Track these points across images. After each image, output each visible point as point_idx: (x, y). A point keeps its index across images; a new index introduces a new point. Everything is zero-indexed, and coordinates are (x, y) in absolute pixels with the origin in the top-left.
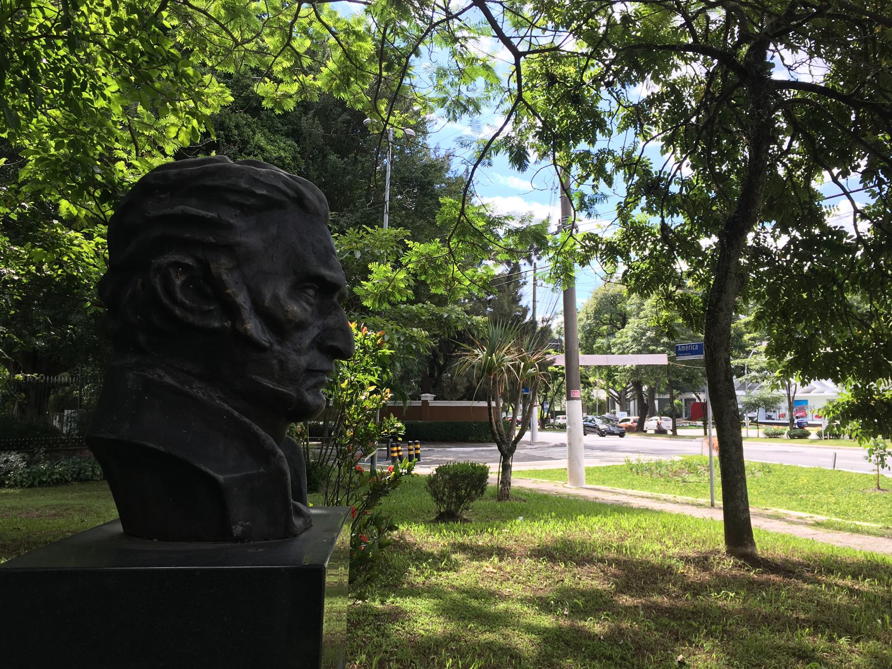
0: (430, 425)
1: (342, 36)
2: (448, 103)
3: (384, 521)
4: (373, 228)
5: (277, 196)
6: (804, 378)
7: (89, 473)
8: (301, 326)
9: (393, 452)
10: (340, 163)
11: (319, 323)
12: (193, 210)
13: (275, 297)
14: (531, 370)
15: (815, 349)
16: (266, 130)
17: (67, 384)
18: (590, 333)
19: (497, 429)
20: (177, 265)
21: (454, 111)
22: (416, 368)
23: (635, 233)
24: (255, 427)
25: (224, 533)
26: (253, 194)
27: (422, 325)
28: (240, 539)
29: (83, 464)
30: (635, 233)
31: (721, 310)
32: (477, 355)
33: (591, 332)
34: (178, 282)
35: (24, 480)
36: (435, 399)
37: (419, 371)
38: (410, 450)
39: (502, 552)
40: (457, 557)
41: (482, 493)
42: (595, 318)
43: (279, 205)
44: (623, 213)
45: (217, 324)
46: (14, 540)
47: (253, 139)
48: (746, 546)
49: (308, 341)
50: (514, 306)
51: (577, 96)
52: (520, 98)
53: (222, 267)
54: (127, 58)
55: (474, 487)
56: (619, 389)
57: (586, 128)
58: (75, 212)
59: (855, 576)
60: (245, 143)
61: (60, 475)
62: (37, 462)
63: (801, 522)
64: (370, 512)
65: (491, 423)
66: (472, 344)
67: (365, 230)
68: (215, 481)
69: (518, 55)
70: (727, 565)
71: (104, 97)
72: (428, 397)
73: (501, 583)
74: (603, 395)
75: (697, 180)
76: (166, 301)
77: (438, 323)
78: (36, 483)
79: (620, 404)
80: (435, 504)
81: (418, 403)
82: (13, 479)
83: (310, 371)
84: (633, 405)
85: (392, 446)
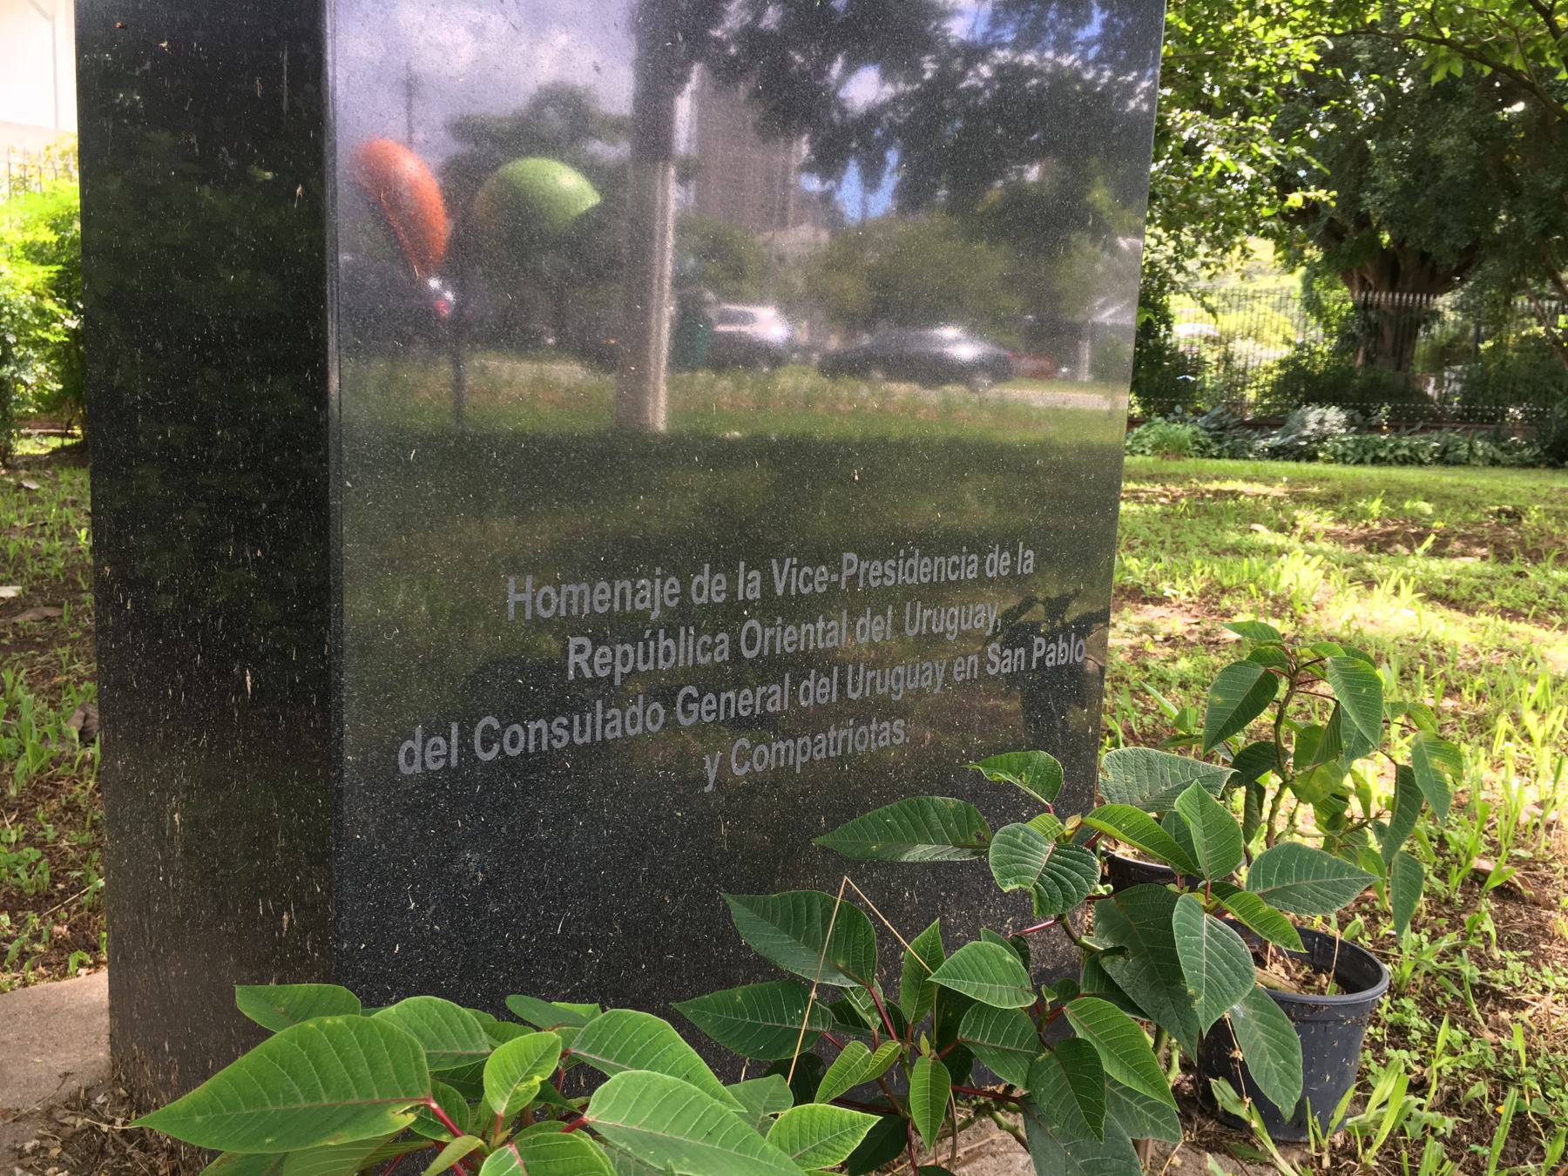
7: (1463, 452)
35: (1349, 452)
61: (1411, 450)
78: (1368, 458)
82: (1331, 450)
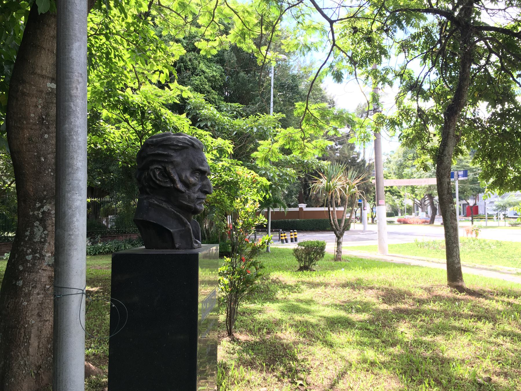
0: (304, 221)
1: (240, 14)
2: (300, 46)
3: (258, 264)
4: (263, 114)
5: (185, 145)
6: (500, 191)
8: (195, 185)
9: (282, 236)
10: (246, 77)
11: (201, 183)
12: (160, 152)
13: (186, 176)
14: (352, 190)
15: (506, 175)
16: (206, 61)
17: (108, 202)
18: (401, 166)
19: (334, 222)
20: (157, 168)
21: (303, 51)
22: (295, 189)
23: (406, 113)
24: (181, 216)
25: (173, 247)
26: (178, 146)
27: (293, 166)
28: (177, 249)
29: (120, 243)
30: (406, 113)
31: (445, 155)
32: (322, 182)
33: (401, 165)
34: (157, 173)
36: (307, 207)
37: (297, 191)
38: (291, 235)
39: (326, 285)
40: (302, 287)
41: (323, 256)
42: (404, 156)
43: (186, 148)
44: (398, 101)
45: (169, 185)
46: (90, 278)
47: (199, 66)
48: (458, 282)
49: (197, 189)
50: (352, 152)
51: (370, 38)
52: (334, 45)
53: (170, 169)
54: (133, 41)
55: (318, 253)
56: (420, 199)
57: (376, 55)
58: (110, 115)
59: (508, 297)
60: (195, 69)
62: (97, 242)
63: (509, 273)
64: (252, 260)
65: (330, 219)
66: (320, 177)
67: (258, 115)
68: (170, 231)
69: (332, 22)
70: (446, 292)
71: (123, 60)
72: (303, 206)
73: (325, 299)
74: (410, 203)
75: (440, 81)
76: (154, 179)
77: (301, 166)
78: (97, 253)
79: (422, 208)
80: (297, 262)
81: (297, 209)
83: (198, 199)
84: (429, 209)
85: (281, 233)
